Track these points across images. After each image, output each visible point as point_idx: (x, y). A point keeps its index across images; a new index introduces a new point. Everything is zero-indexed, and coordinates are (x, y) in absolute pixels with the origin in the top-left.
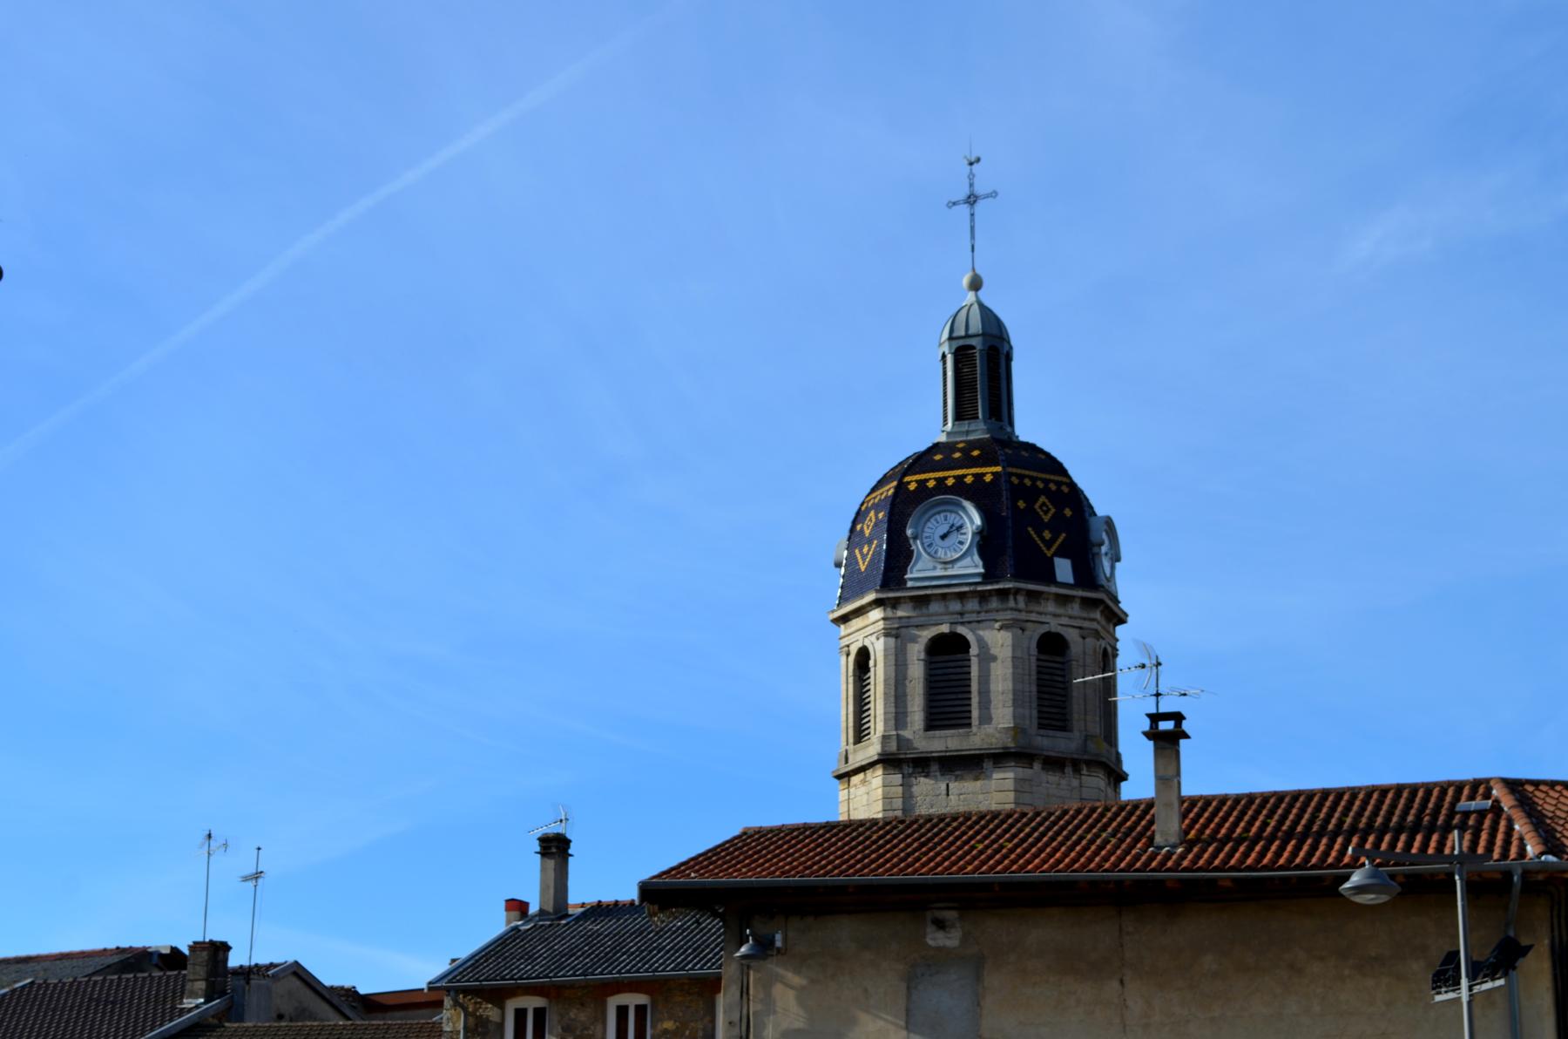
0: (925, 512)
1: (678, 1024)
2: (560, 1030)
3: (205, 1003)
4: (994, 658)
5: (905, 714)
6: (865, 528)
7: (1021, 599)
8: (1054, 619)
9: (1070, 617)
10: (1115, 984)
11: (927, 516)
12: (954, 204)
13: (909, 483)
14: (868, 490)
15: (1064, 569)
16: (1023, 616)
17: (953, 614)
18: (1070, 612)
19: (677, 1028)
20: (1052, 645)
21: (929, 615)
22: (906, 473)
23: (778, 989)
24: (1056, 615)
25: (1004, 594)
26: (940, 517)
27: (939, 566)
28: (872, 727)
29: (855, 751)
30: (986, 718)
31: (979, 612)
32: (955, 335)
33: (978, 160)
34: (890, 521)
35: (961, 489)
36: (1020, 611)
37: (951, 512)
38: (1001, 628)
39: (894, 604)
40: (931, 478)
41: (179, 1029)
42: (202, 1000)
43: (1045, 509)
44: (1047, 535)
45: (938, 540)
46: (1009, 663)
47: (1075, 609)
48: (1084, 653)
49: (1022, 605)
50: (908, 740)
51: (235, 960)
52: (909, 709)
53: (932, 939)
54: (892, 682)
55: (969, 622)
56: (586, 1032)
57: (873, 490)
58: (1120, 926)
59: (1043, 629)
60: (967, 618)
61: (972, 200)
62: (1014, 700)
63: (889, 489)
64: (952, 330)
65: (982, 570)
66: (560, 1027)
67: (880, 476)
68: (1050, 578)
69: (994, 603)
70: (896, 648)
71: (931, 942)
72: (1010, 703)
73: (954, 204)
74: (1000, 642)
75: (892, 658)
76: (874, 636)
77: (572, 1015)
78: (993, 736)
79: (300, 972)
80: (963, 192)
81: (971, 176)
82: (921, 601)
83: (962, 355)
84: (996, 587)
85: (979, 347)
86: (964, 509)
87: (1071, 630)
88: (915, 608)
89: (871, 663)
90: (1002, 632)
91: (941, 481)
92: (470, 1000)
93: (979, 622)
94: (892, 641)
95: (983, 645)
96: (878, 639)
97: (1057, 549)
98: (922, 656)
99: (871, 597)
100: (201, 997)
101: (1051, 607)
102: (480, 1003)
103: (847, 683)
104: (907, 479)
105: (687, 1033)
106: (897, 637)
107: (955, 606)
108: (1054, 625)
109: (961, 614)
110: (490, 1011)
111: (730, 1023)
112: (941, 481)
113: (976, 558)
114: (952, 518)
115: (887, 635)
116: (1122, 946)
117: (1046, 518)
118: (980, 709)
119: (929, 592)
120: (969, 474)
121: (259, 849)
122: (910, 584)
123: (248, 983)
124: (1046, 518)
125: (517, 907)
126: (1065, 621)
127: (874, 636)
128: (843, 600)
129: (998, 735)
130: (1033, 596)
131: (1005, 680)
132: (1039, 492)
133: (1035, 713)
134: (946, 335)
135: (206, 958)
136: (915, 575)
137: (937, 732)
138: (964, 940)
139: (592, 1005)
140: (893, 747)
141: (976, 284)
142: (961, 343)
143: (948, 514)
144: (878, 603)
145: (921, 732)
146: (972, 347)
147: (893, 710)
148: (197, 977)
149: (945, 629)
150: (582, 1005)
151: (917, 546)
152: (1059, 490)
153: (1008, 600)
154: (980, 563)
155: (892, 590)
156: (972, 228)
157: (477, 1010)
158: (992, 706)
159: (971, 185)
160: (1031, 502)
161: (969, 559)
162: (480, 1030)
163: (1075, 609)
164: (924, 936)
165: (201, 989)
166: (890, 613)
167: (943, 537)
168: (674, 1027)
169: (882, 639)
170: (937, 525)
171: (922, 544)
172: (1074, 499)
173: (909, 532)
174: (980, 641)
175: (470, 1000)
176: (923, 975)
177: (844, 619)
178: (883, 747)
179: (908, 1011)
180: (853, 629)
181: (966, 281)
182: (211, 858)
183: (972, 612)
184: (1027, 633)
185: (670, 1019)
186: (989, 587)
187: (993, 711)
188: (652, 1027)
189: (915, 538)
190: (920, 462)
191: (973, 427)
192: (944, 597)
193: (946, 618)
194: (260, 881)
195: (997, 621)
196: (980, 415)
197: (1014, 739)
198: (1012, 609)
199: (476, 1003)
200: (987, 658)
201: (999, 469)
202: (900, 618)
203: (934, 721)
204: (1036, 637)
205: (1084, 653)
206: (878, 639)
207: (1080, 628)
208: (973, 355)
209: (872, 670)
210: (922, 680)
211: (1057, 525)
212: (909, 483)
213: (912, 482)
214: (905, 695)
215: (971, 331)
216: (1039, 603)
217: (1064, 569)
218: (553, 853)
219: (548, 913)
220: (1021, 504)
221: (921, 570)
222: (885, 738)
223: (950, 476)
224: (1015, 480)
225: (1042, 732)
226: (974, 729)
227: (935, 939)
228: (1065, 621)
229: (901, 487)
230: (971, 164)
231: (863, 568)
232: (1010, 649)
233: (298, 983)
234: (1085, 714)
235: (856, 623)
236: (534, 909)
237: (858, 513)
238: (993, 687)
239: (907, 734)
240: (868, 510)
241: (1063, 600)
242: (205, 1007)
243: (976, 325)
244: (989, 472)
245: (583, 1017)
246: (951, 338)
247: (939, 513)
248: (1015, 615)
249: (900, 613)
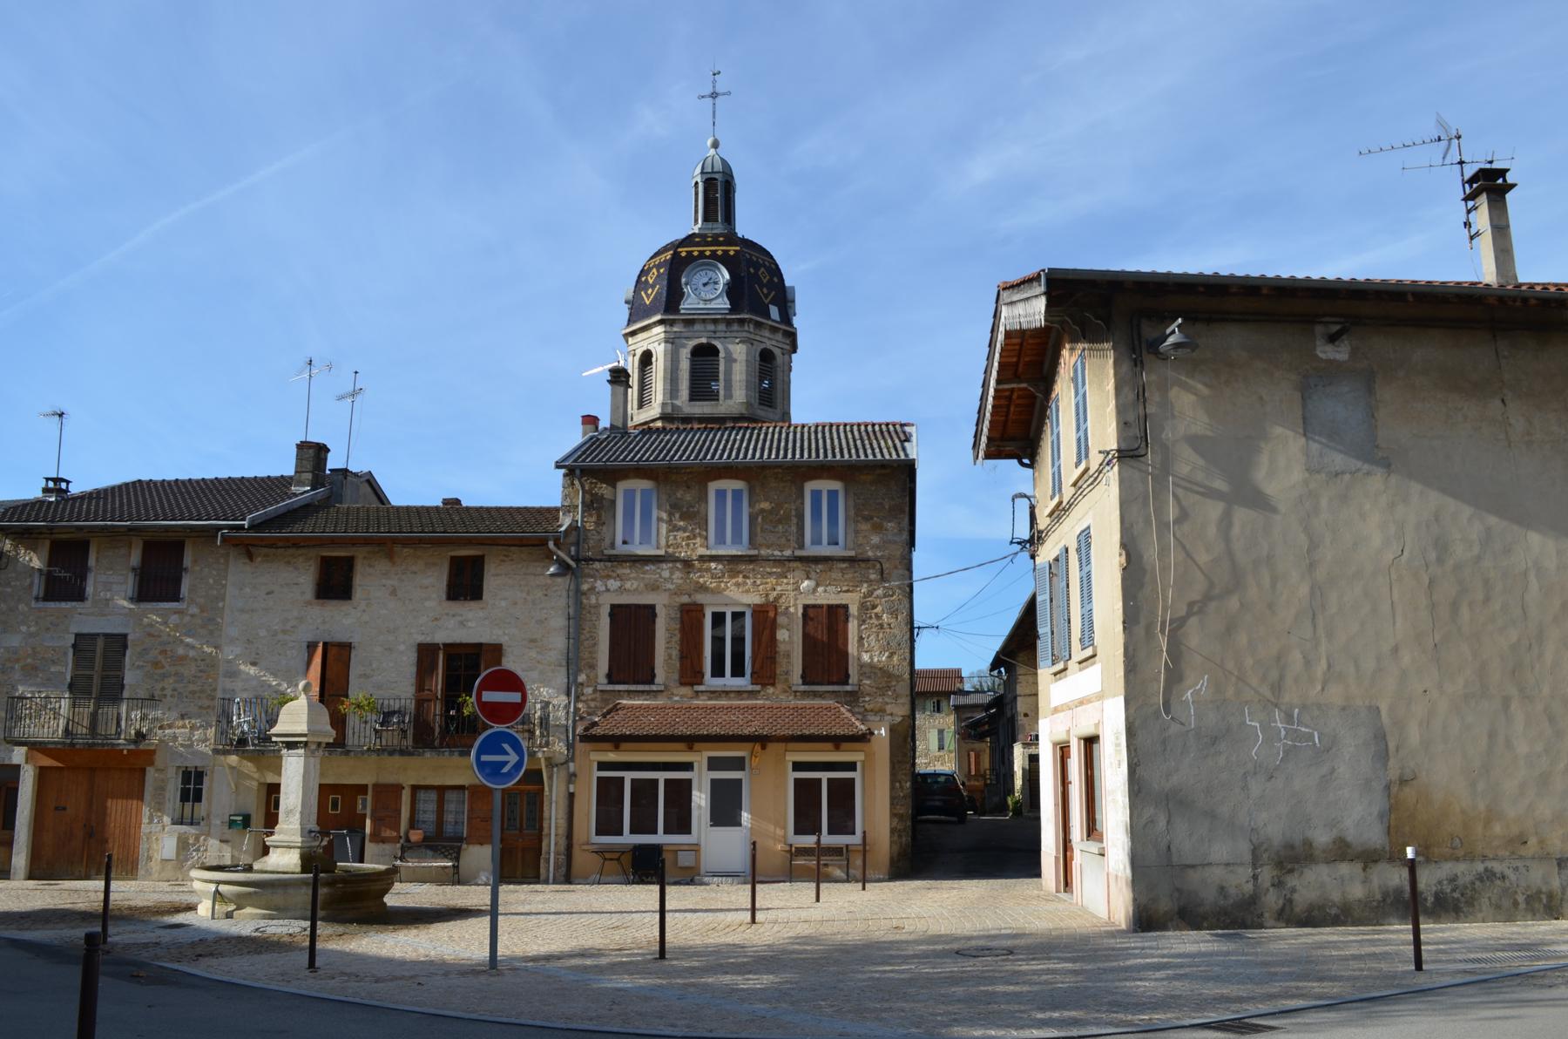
0: (693, 269)
1: (773, 505)
2: (668, 507)
3: (312, 490)
4: (735, 361)
5: (677, 391)
6: (649, 278)
7: (751, 326)
8: (772, 342)
9: (777, 341)
10: (1498, 403)
11: (694, 272)
12: (703, 97)
13: (681, 252)
14: (648, 258)
15: (774, 312)
16: (752, 336)
17: (709, 331)
18: (777, 338)
19: (773, 508)
20: (766, 357)
21: (694, 332)
22: (679, 246)
23: (1174, 392)
24: (769, 339)
25: (741, 322)
26: (703, 273)
27: (701, 302)
28: (653, 398)
29: (638, 413)
30: (729, 396)
31: (726, 332)
32: (705, 171)
33: (719, 73)
34: (670, 274)
36: (750, 333)
37: (710, 270)
38: (740, 342)
39: (671, 323)
40: (696, 251)
41: (299, 505)
42: (309, 488)
44: (765, 291)
45: (701, 287)
46: (744, 364)
47: (779, 336)
48: (784, 363)
49: (752, 330)
50: (679, 407)
51: (333, 462)
52: (680, 388)
53: (1321, 352)
54: (669, 371)
55: (720, 338)
56: (691, 510)
57: (652, 258)
58: (1496, 350)
59: (763, 346)
60: (718, 335)
61: (714, 95)
62: (747, 386)
63: (668, 255)
64: (703, 168)
65: (729, 307)
66: (668, 504)
67: (652, 254)
68: (767, 315)
69: (735, 327)
70: (672, 350)
71: (1321, 355)
72: (744, 388)
73: (703, 97)
74: (739, 351)
75: (669, 356)
76: (657, 343)
77: (679, 495)
78: (733, 407)
79: (372, 480)
81: (714, 82)
82: (689, 323)
83: (709, 183)
84: (738, 317)
85: (720, 179)
86: (719, 269)
87: (777, 349)
88: (685, 327)
89: (654, 359)
90: (740, 345)
91: (701, 253)
92: (586, 480)
93: (725, 338)
94: (669, 346)
95: (728, 353)
96: (659, 344)
97: (772, 299)
98: (689, 356)
99: (658, 317)
100: (308, 486)
101: (767, 333)
102: (596, 483)
104: (680, 250)
105: (782, 512)
106: (672, 343)
107: (711, 327)
108: (769, 344)
109: (715, 332)
110: (604, 490)
111: (1125, 423)
112: (701, 253)
113: (726, 299)
114: (710, 274)
115: (666, 342)
116: (1500, 368)
117: (765, 281)
118: (725, 390)
119: (695, 317)
121: (356, 372)
122: (682, 311)
123: (346, 478)
124: (765, 281)
125: (590, 420)
126: (774, 343)
127: (657, 343)
128: (630, 322)
129: (736, 406)
131: (741, 373)
132: (761, 266)
133: (757, 395)
134: (698, 170)
135: (313, 455)
136: (686, 306)
137: (697, 403)
138: (1354, 353)
139: (697, 487)
141: (715, 145)
142: (709, 176)
143: (708, 272)
144: (661, 322)
145: (687, 402)
146: (715, 179)
147: (669, 388)
148: (304, 470)
149: (704, 340)
150: (688, 487)
151: (687, 290)
152: (770, 266)
153: (744, 325)
154: (728, 302)
155: (671, 314)
156: (714, 112)
157: (593, 489)
158: (733, 389)
159: (714, 87)
160: (757, 269)
161: (721, 299)
162: (595, 505)
164: (1315, 348)
165: (308, 479)
166: (668, 329)
167: (705, 285)
168: (770, 507)
169: (663, 345)
170: (701, 277)
171: (691, 288)
173: (683, 280)
174: (726, 350)
175: (586, 480)
176: (1316, 386)
177: (633, 333)
178: (662, 409)
179: (1304, 419)
180: (639, 340)
181: (709, 142)
182: (312, 379)
183: (721, 331)
184: (754, 347)
185: (766, 500)
186: (734, 317)
187: (733, 392)
188: (750, 505)
189: (686, 284)
190: (689, 240)
191: (715, 226)
192: (704, 321)
193: (705, 334)
194: (358, 398)
195: (737, 338)
196: (720, 220)
197: (747, 409)
198: (746, 331)
199: (591, 483)
200: (730, 360)
201: (738, 248)
202: (676, 332)
203: (695, 396)
204: (759, 350)
205: (784, 363)
206: (659, 344)
207: (782, 349)
208: (716, 185)
209: (654, 364)
210: (688, 371)
212: (681, 252)
213: (683, 252)
214: (677, 379)
215: (715, 170)
216: (760, 330)
217: (774, 312)
218: (623, 381)
219: (618, 428)
220: (752, 270)
221: (690, 303)
222: (664, 405)
223: (708, 250)
224: (748, 257)
225: (762, 407)
226: (721, 402)
227: (1326, 352)
228: (774, 343)
229: (676, 255)
230: (714, 75)
231: (648, 303)
232: (745, 355)
233: (369, 489)
234: (783, 400)
235: (640, 336)
236: (605, 423)
237: (642, 271)
238: (733, 377)
239: (678, 403)
240: (650, 269)
241: (774, 330)
242: (312, 493)
243: (719, 167)
244: (732, 250)
245: (688, 497)
246: (702, 173)
247: (702, 270)
248: (748, 335)
249: (675, 329)
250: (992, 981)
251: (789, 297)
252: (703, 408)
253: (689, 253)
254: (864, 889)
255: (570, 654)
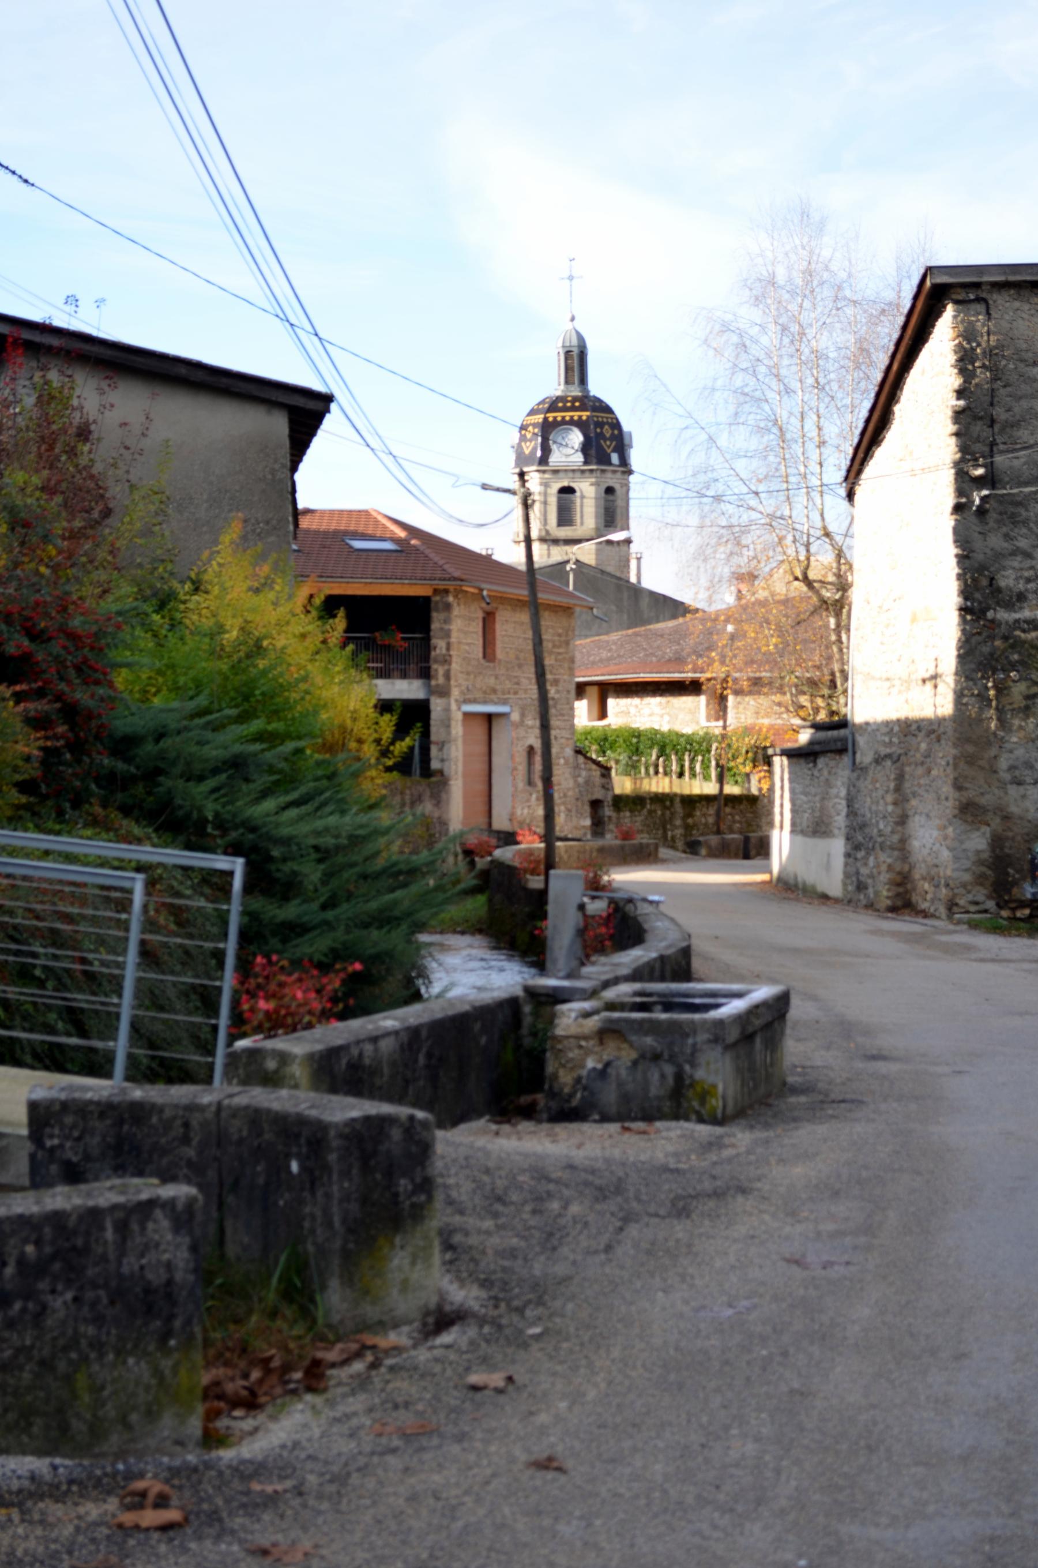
8: (611, 480)
15: (615, 458)
20: (610, 490)
25: (591, 471)
35: (572, 422)
39: (544, 472)
43: (607, 431)
47: (619, 475)
68: (609, 463)
80: (567, 274)
82: (556, 472)
83: (568, 354)
103: (36, 296)
108: (611, 483)
120: (576, 415)
130: (603, 471)
140: (543, 533)
141: (573, 319)
160: (602, 428)
163: (619, 475)
172: (616, 425)
211: (613, 437)
217: (615, 458)
221: (557, 458)
223: (568, 415)
241: (614, 472)
243: (575, 341)
244: (585, 415)
250: (694, 996)
251: (626, 441)
252: (564, 533)
253: (555, 418)
254: (581, 277)
255: (561, 819)
